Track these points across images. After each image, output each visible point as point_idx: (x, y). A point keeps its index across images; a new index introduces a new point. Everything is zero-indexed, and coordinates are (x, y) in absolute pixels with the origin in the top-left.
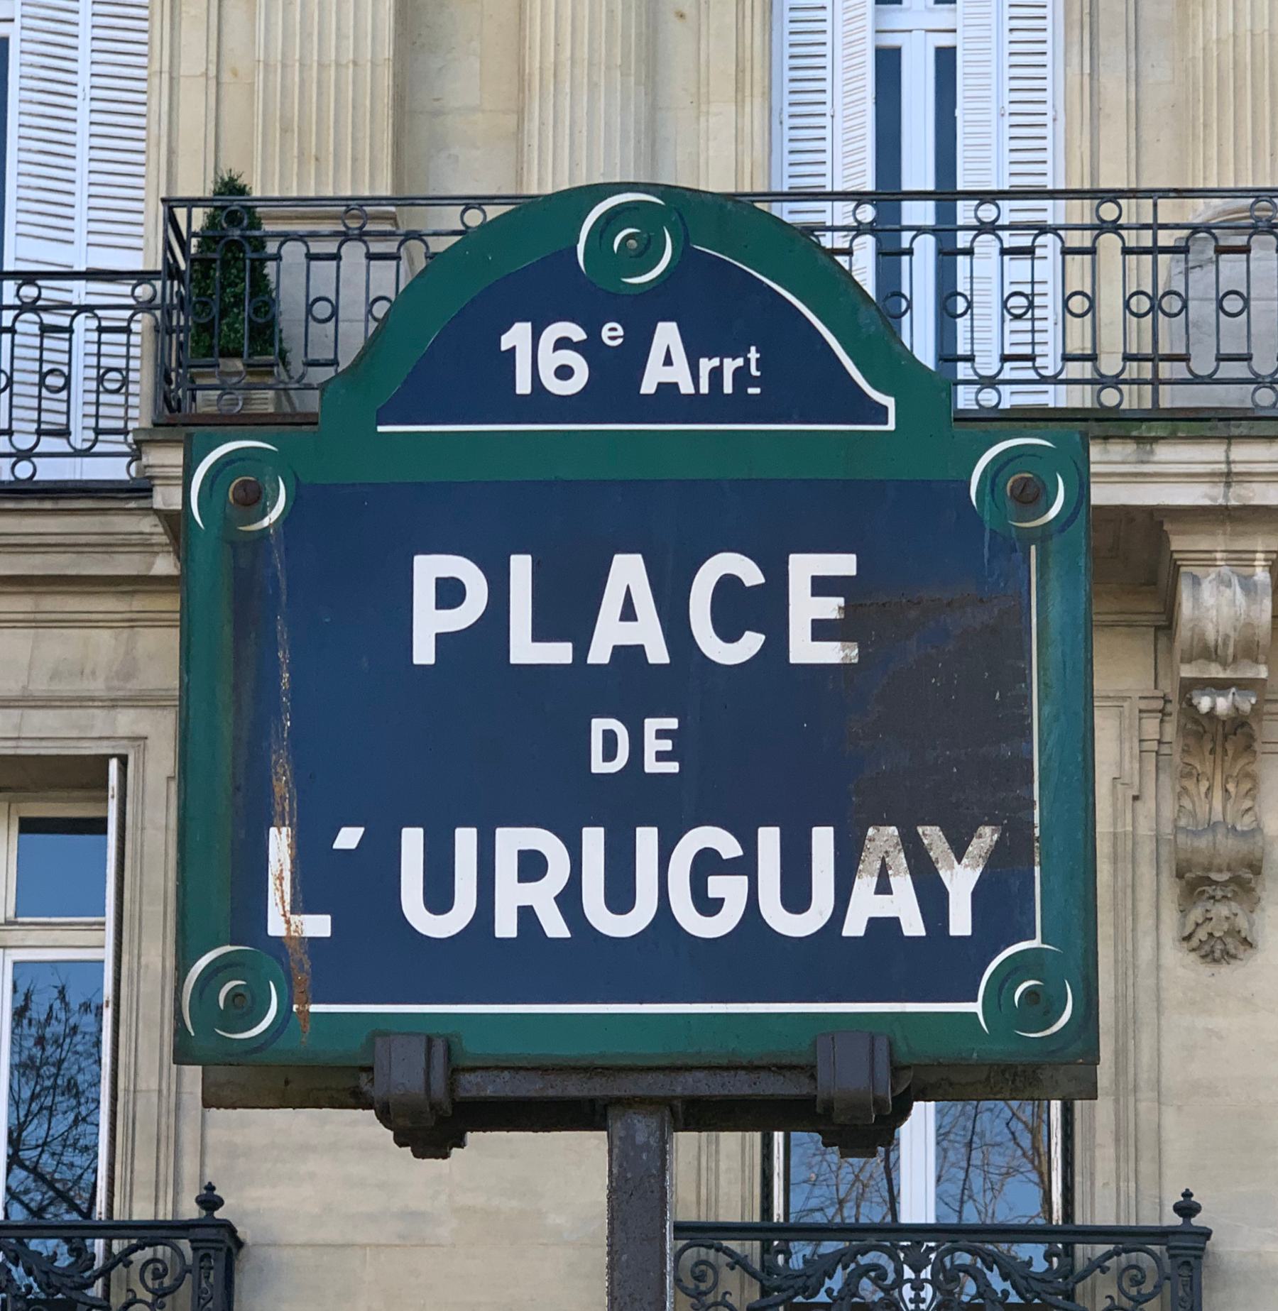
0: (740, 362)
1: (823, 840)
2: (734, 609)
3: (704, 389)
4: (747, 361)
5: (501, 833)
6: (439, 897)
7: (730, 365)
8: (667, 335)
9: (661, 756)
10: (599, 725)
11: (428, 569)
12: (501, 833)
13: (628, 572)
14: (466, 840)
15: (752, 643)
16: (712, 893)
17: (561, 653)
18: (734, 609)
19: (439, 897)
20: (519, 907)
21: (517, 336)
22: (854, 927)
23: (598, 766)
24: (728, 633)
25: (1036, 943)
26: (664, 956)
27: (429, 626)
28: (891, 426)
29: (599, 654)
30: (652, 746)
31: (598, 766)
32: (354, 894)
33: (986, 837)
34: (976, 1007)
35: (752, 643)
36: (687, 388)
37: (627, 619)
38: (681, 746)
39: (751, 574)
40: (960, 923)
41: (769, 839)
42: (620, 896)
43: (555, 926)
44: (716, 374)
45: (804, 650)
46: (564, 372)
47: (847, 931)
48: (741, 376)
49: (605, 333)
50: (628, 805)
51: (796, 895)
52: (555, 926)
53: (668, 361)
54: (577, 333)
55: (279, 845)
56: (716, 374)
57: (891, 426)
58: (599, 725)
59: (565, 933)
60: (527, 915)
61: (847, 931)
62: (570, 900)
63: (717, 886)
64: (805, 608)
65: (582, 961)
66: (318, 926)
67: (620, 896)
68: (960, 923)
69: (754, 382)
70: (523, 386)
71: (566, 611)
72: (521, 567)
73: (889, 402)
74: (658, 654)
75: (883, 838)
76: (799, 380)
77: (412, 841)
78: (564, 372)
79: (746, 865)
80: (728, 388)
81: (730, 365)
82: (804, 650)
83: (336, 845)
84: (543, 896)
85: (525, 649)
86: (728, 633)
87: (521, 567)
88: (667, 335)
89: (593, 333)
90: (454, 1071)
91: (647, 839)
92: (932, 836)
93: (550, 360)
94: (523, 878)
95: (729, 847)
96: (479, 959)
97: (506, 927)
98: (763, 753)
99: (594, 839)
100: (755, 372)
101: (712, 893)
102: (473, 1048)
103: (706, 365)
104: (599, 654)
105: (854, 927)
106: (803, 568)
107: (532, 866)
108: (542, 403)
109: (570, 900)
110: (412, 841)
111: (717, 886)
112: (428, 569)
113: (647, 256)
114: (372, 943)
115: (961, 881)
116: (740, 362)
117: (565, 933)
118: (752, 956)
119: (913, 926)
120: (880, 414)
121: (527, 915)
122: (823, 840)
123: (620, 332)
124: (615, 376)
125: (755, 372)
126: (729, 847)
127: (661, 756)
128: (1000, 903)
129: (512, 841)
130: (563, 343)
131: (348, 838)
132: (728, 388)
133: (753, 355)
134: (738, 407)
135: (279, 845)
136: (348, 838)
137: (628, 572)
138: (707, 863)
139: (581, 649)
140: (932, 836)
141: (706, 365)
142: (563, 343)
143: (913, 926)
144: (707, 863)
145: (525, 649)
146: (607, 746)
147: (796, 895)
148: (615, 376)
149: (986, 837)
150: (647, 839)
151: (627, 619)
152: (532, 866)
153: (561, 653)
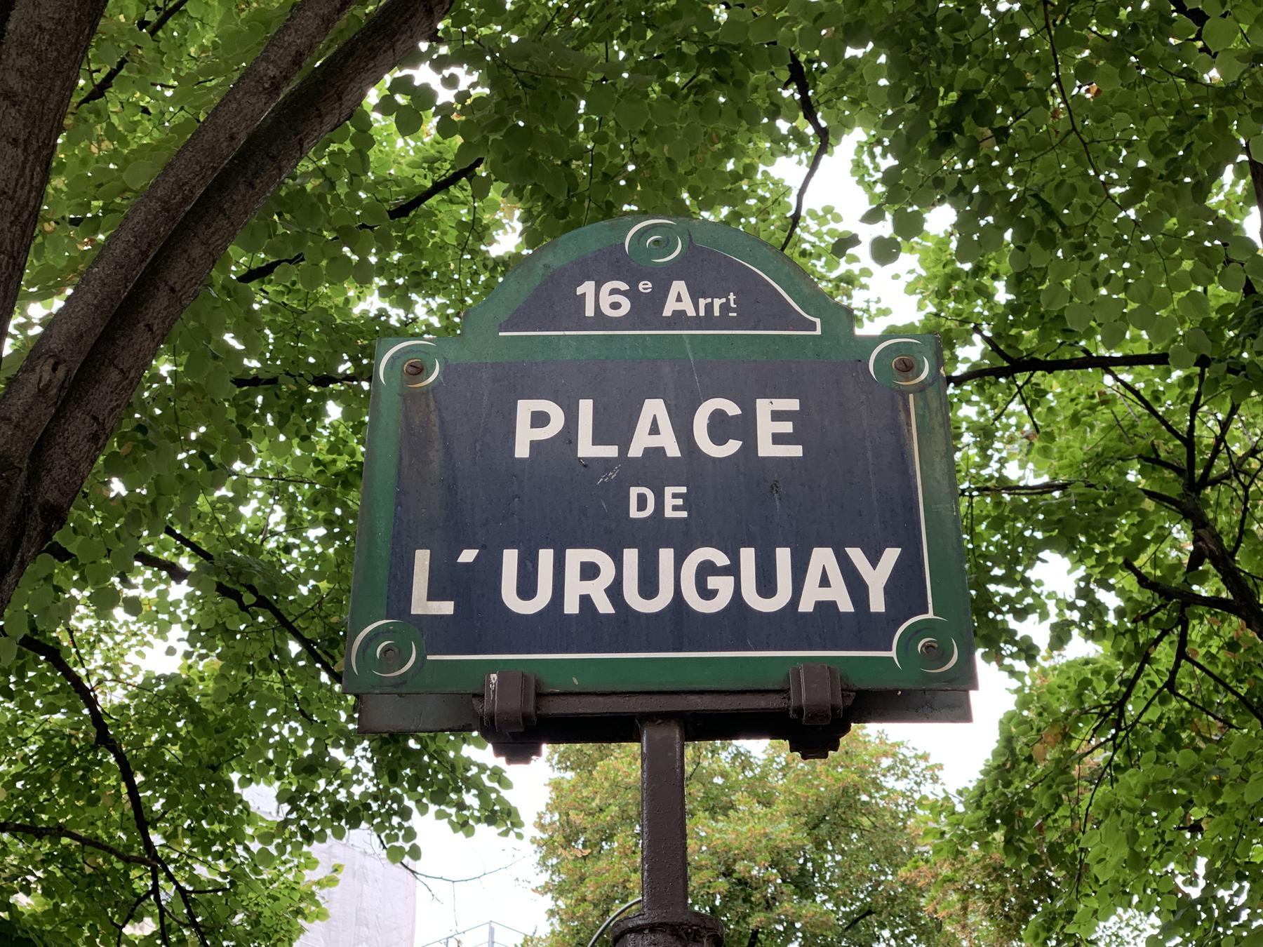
0: (724, 300)
1: (783, 556)
2: (720, 427)
3: (702, 313)
4: (728, 300)
5: (569, 552)
6: (527, 589)
7: (717, 302)
8: (679, 287)
9: (675, 508)
10: (634, 492)
11: (525, 408)
12: (569, 552)
13: (654, 408)
14: (546, 557)
15: (733, 446)
16: (710, 587)
17: (611, 451)
18: (720, 427)
19: (527, 589)
20: (532, 442)
21: (587, 288)
22: (806, 606)
23: (634, 513)
24: (718, 437)
25: (930, 615)
26: (679, 624)
27: (524, 439)
28: (818, 332)
29: (635, 451)
30: (669, 502)
31: (634, 513)
32: (472, 590)
33: (891, 556)
34: (893, 654)
35: (733, 446)
36: (691, 312)
37: (654, 428)
38: (688, 502)
39: (732, 409)
40: (877, 603)
41: (748, 556)
42: (649, 587)
43: (604, 606)
44: (709, 307)
45: (766, 449)
46: (616, 306)
47: (801, 609)
48: (725, 308)
49: (641, 286)
50: (650, 537)
51: (767, 586)
52: (604, 606)
53: (678, 299)
54: (623, 286)
55: (422, 559)
56: (709, 307)
57: (818, 332)
58: (634, 492)
59: (611, 610)
60: (586, 601)
61: (801, 609)
62: (615, 591)
63: (712, 582)
64: (766, 427)
65: (624, 627)
66: (446, 608)
67: (649, 587)
68: (877, 603)
69: (733, 310)
70: (590, 312)
71: (615, 426)
72: (586, 408)
73: (818, 321)
74: (673, 451)
75: (822, 557)
76: (760, 306)
77: (510, 558)
78: (616, 306)
79: (733, 570)
80: (717, 313)
81: (717, 302)
82: (766, 449)
83: (460, 560)
84: (597, 591)
85: (587, 448)
86: (718, 437)
87: (586, 408)
88: (679, 287)
89: (633, 285)
90: (540, 695)
91: (666, 556)
92: (856, 555)
93: (606, 300)
94: (584, 579)
95: (721, 559)
96: (554, 627)
97: (571, 606)
98: (743, 507)
99: (631, 557)
100: (732, 305)
101: (710, 587)
102: (554, 683)
103: (702, 302)
104: (635, 451)
105: (806, 606)
106: (764, 407)
107: (590, 572)
108: (600, 320)
109: (615, 591)
110: (510, 558)
111: (712, 582)
112: (525, 408)
113: (667, 246)
114: (479, 616)
115: (877, 577)
116: (724, 300)
117: (611, 610)
118: (738, 623)
119: (846, 606)
120: (812, 326)
121: (586, 601)
122: (783, 556)
123: (650, 285)
124: (647, 309)
125: (732, 305)
126: (721, 559)
127: (675, 508)
128: (904, 588)
129: (575, 557)
130: (614, 291)
131: (468, 556)
132: (717, 313)
133: (732, 297)
134: (724, 322)
135: (422, 559)
136: (468, 556)
137: (654, 408)
138: (707, 569)
139: (624, 446)
140: (856, 555)
141: (702, 302)
142: (614, 291)
143: (846, 606)
144: (707, 569)
145: (587, 448)
146: (639, 504)
147: (767, 586)
148: (647, 309)
149: (891, 556)
150: (666, 556)
151: (654, 428)
152: (590, 572)
153: (611, 451)
